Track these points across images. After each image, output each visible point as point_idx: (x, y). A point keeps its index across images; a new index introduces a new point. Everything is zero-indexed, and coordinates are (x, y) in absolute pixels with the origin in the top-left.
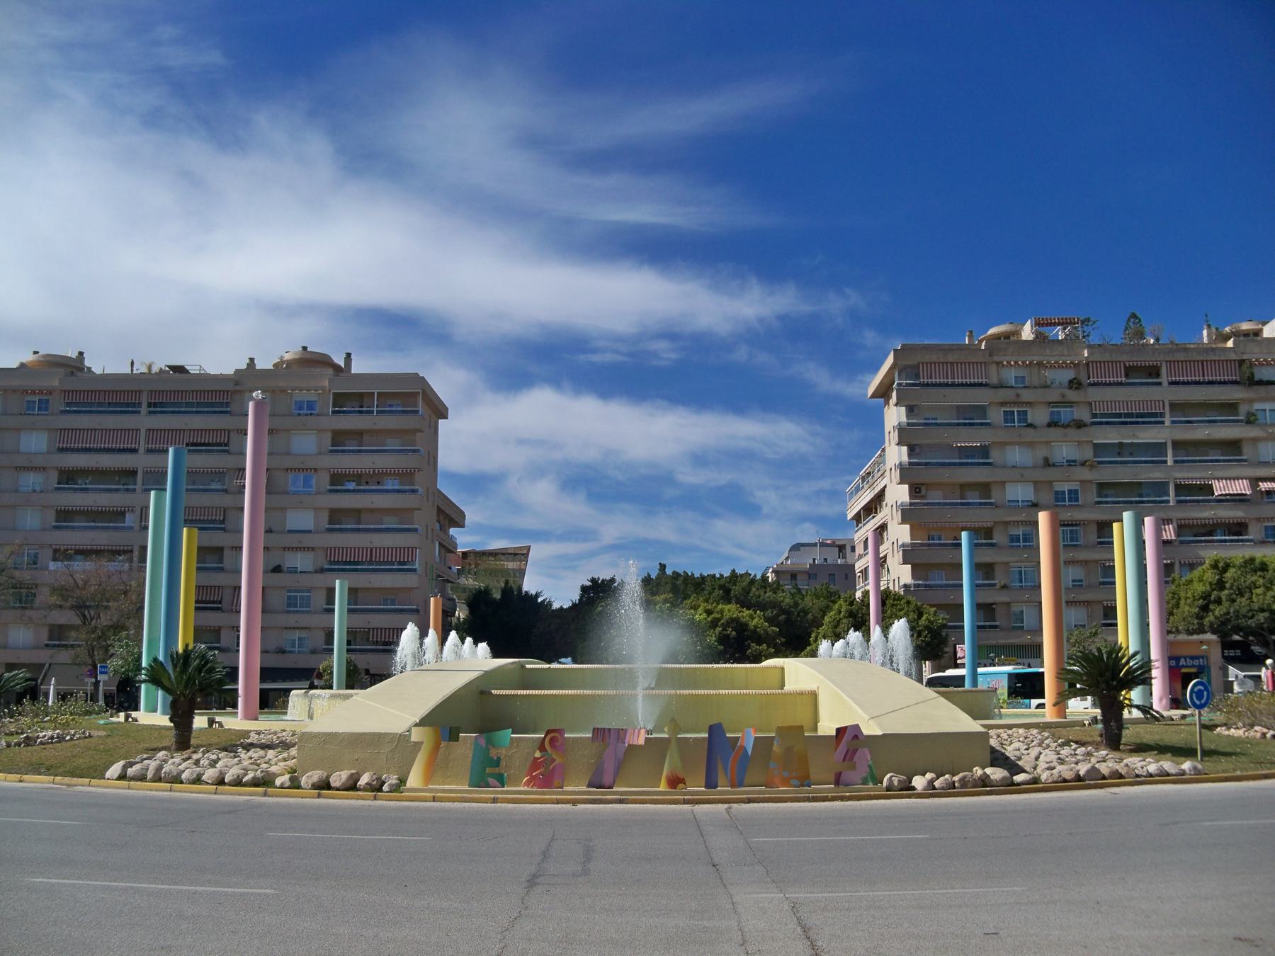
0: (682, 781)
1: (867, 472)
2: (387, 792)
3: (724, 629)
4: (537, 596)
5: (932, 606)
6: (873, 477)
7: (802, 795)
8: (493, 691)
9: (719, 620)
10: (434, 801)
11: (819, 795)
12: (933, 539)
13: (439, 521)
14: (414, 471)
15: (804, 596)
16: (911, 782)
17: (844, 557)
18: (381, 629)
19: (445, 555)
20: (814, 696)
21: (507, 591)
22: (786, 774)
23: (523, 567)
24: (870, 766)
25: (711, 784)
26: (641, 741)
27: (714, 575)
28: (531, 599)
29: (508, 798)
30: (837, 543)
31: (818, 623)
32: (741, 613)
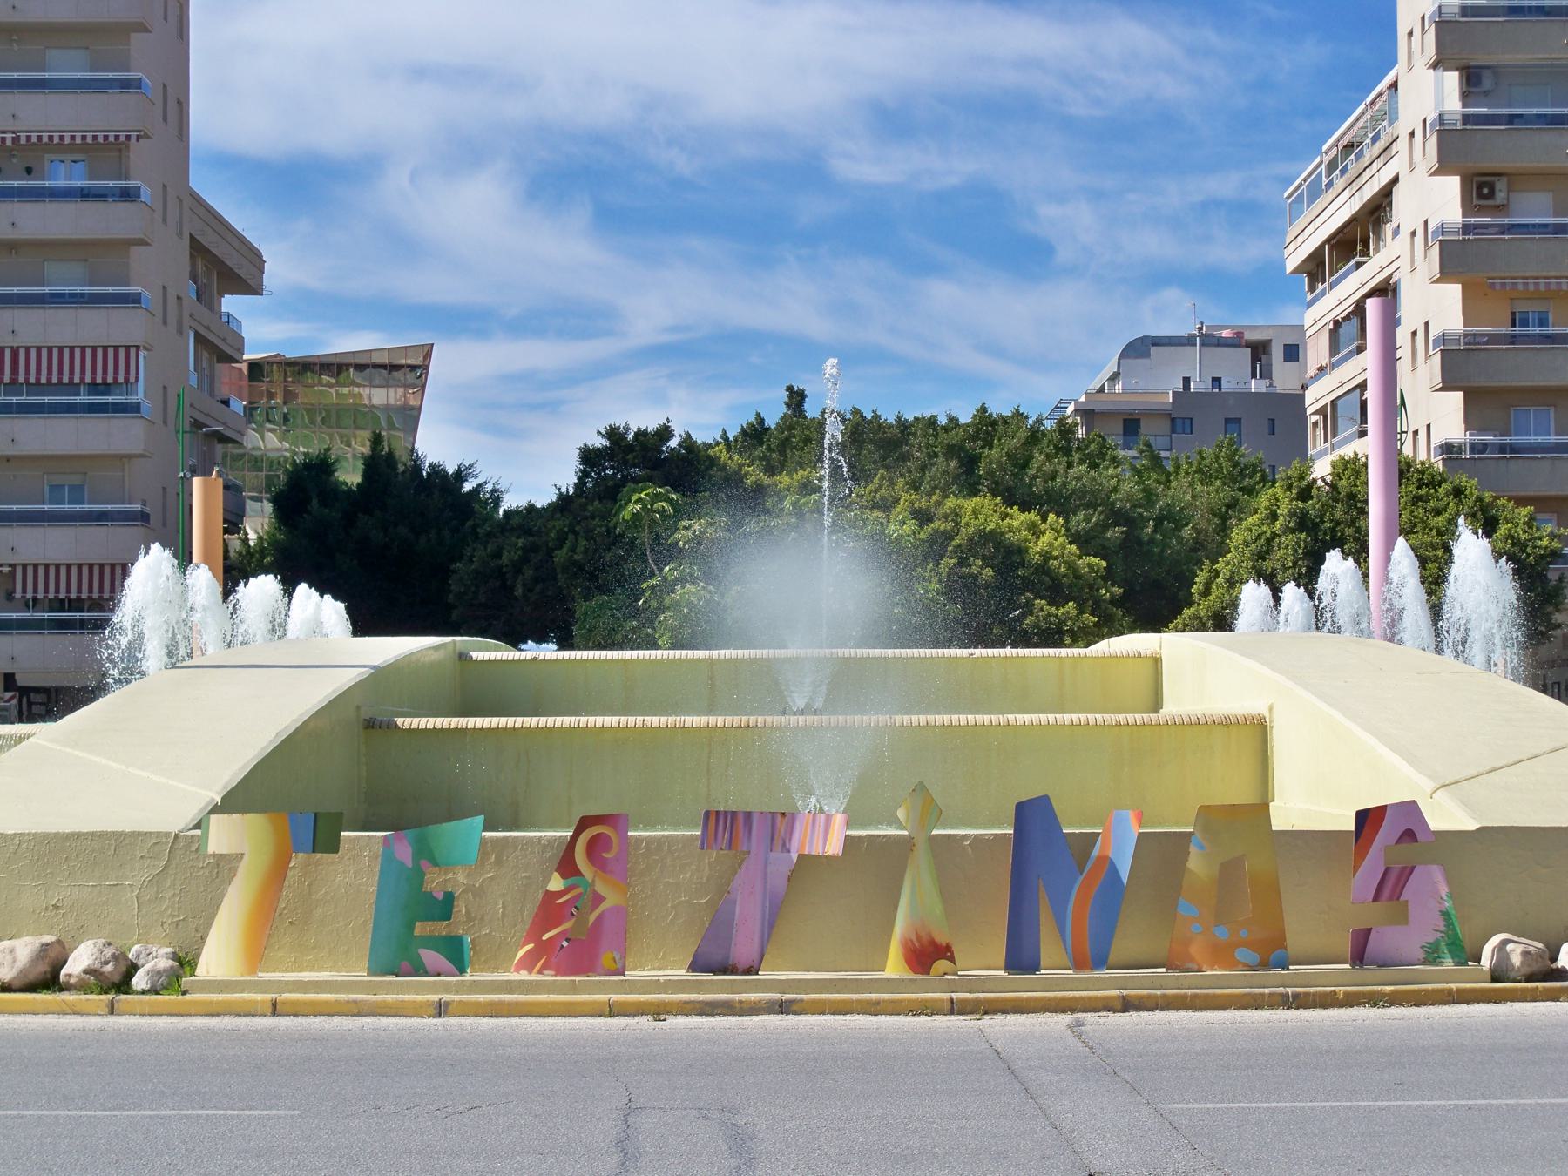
0: (945, 952)
1: (1345, 141)
2: (144, 992)
3: (962, 562)
4: (460, 476)
5: (1521, 501)
6: (1359, 156)
7: (1266, 991)
8: (400, 721)
9: (949, 537)
10: (274, 1013)
11: (1312, 990)
12: (1525, 323)
13: (194, 278)
14: (128, 138)
15: (1168, 475)
16: (1554, 959)
17: (1267, 374)
18: (47, 566)
19: (212, 369)
20: (1259, 730)
21: (379, 465)
22: (1222, 933)
23: (412, 403)
24: (1446, 915)
25: (1021, 959)
26: (834, 847)
27: (932, 421)
28: (444, 485)
29: (478, 1004)
30: (1250, 336)
31: (1210, 547)
32: (1008, 520)
